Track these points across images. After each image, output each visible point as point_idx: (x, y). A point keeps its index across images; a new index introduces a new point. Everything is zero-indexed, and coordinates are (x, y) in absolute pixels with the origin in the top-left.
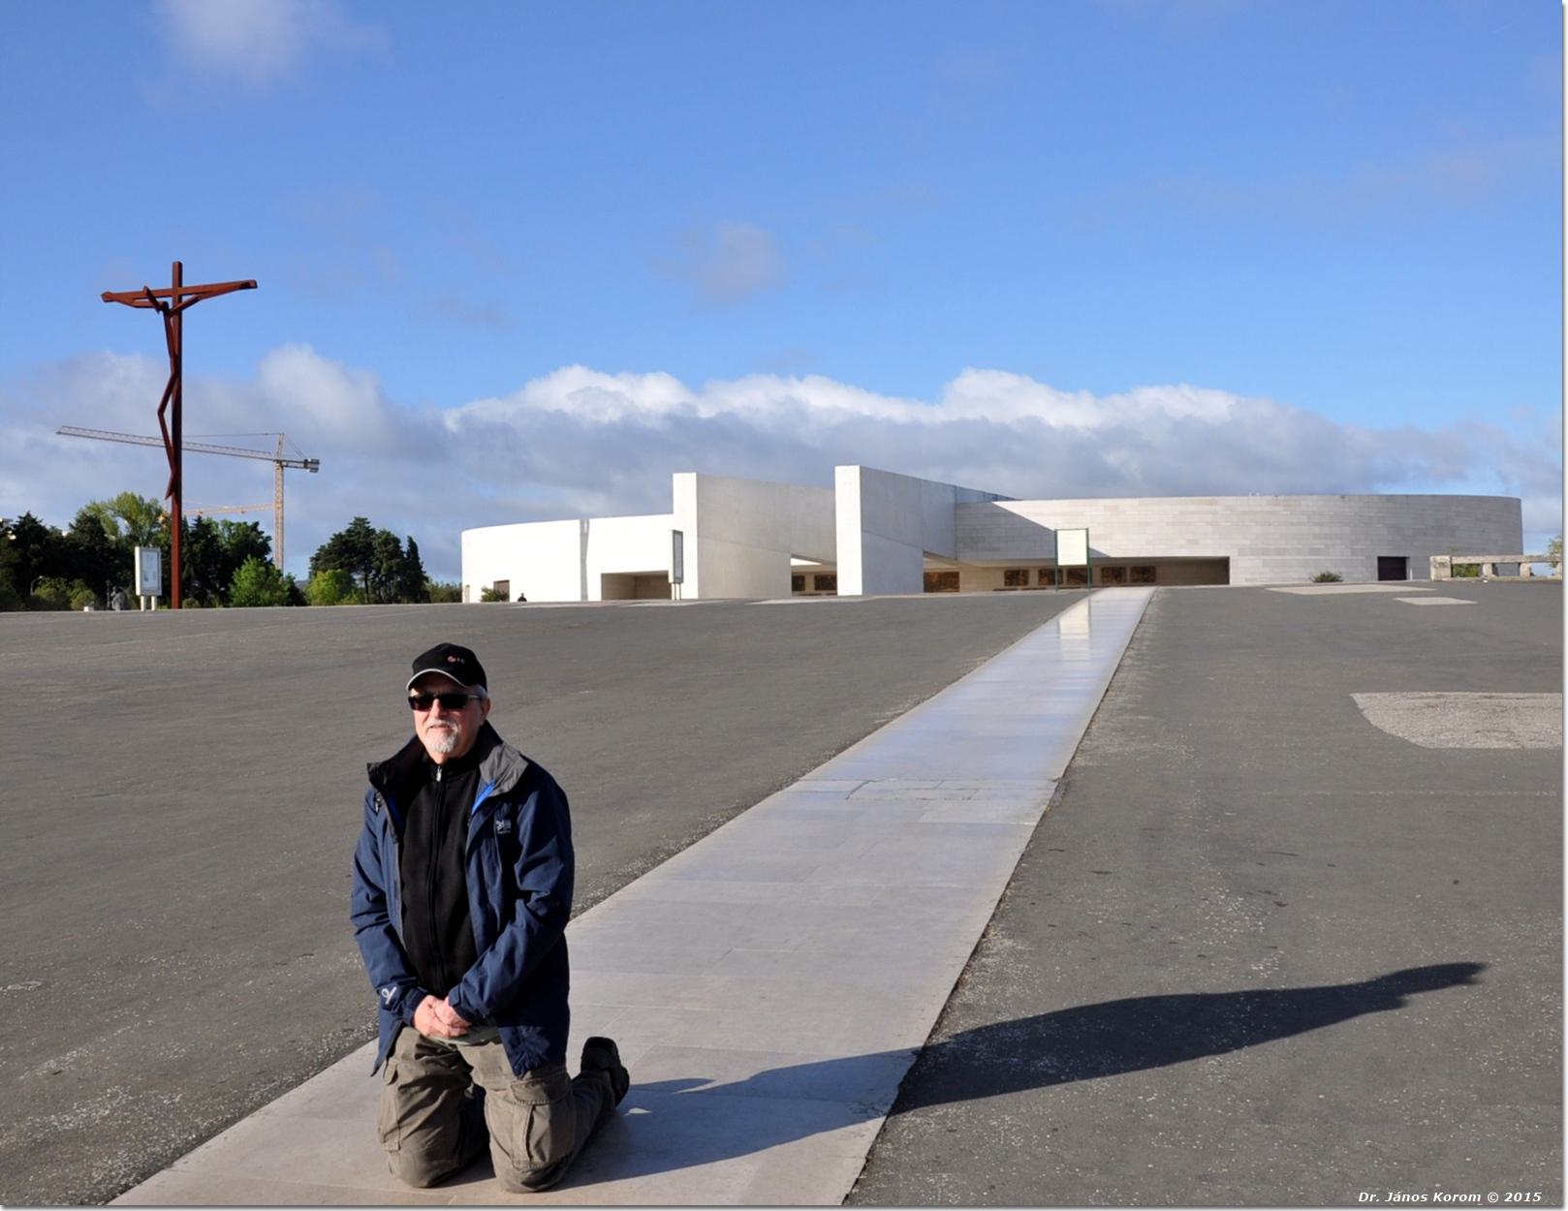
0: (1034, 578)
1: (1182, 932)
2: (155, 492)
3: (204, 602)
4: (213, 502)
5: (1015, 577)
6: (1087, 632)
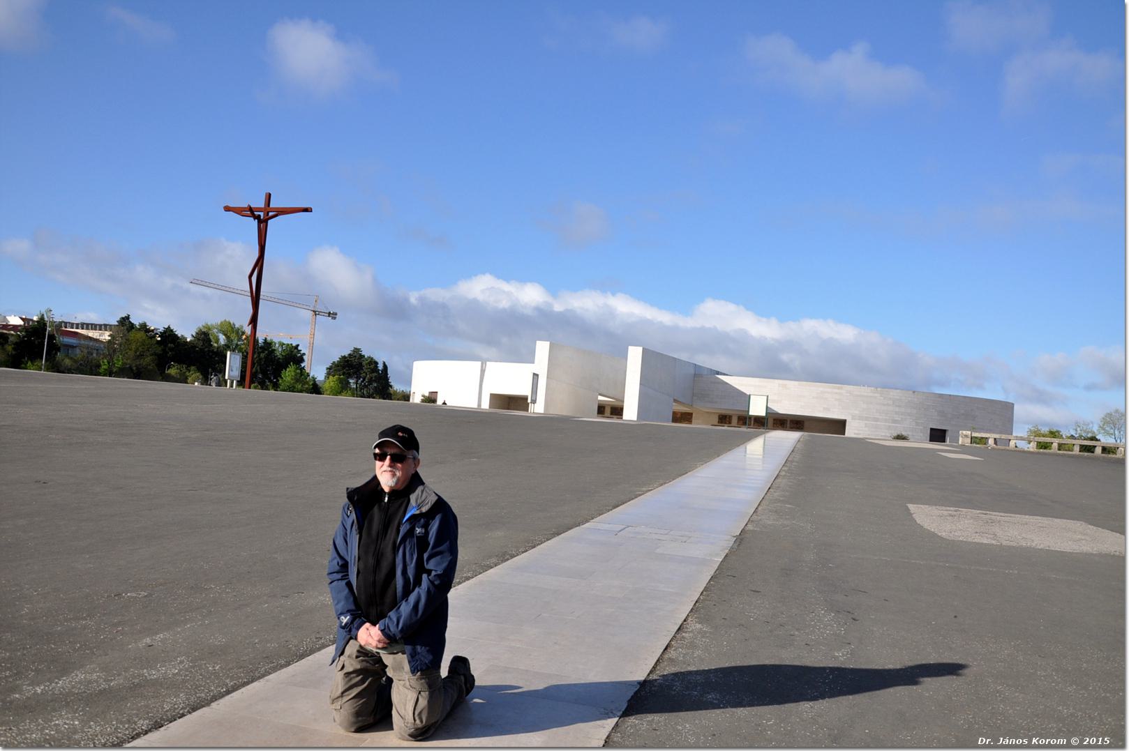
0: (735, 420)
2: (243, 322)
3: (263, 386)
4: (276, 329)
5: (724, 419)
6: (762, 454)
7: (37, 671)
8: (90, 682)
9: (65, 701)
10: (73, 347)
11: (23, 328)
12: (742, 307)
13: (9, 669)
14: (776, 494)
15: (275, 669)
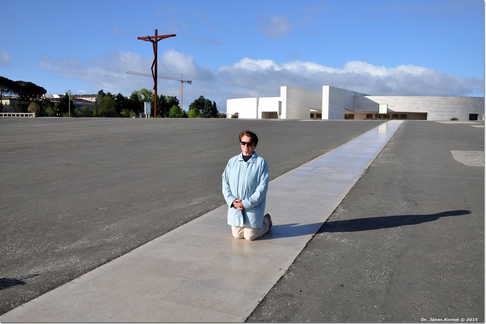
0: (374, 117)
1: (388, 210)
2: (151, 88)
3: (163, 116)
4: (166, 91)
5: (369, 116)
6: (385, 130)
7: (65, 241)
8: (84, 244)
9: (74, 252)
10: (80, 105)
11: (60, 99)
12: (366, 63)
13: (54, 240)
14: (387, 149)
15: (158, 236)
